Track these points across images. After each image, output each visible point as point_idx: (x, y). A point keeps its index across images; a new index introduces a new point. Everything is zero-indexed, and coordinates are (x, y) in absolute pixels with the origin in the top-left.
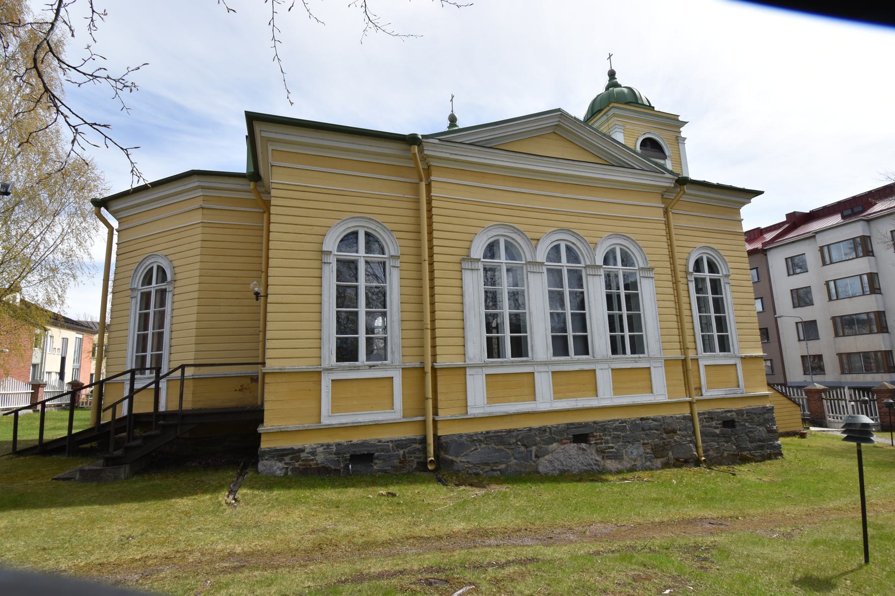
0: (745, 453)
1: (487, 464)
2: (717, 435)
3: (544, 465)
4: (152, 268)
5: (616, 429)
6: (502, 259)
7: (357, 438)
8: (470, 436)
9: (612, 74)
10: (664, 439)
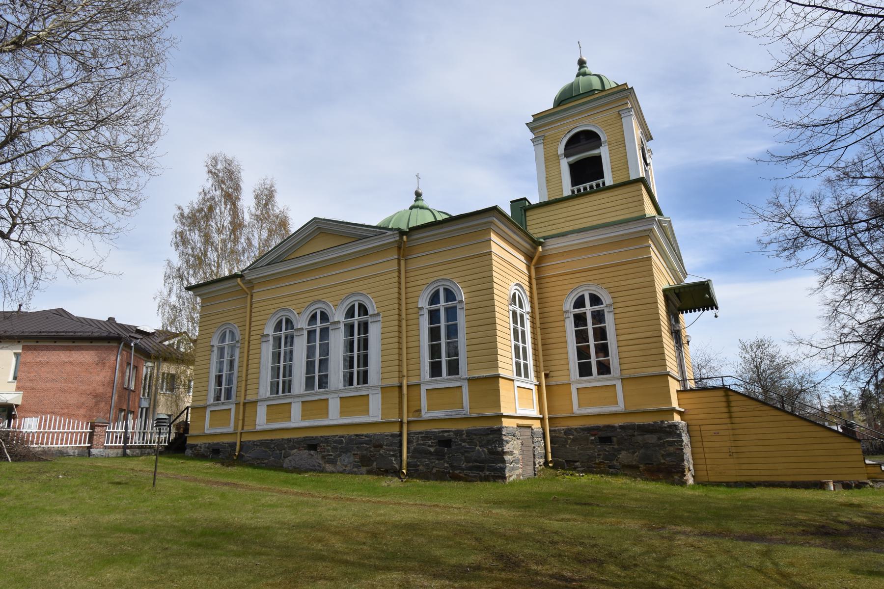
0: (457, 472)
2: (430, 453)
3: (286, 463)
5: (335, 442)
6: (442, 304)
7: (216, 440)
8: (254, 442)
9: (582, 63)
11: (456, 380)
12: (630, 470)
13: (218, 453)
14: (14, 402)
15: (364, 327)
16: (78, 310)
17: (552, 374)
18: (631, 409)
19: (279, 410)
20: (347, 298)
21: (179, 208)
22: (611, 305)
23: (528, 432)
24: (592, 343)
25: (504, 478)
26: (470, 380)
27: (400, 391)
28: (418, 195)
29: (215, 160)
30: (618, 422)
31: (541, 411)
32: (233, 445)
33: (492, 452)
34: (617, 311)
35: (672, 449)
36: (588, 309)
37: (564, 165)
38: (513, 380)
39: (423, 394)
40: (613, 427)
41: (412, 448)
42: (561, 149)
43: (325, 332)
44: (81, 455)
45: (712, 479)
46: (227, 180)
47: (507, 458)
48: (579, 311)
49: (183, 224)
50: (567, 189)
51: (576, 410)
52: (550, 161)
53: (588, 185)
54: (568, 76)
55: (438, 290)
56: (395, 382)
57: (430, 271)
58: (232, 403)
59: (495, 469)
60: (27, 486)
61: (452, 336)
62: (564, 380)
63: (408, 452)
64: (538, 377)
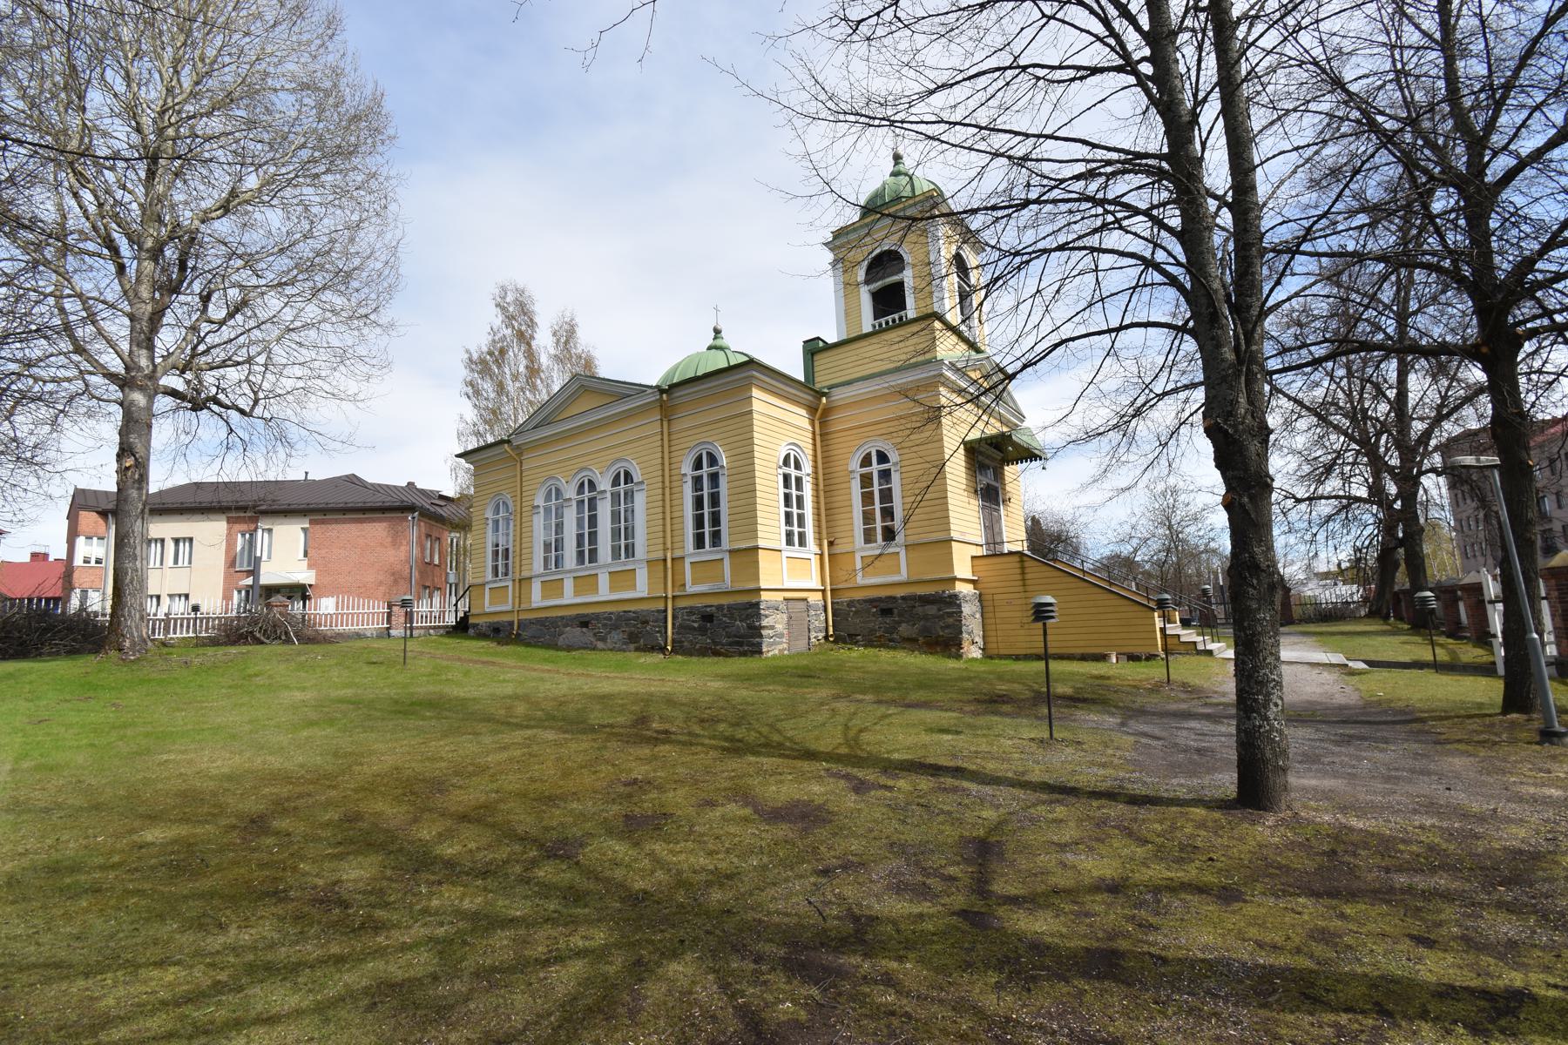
3: (561, 641)
7: (496, 619)
12: (910, 643)
13: (499, 633)
14: (307, 582)
16: (372, 475)
18: (913, 579)
19: (552, 587)
20: (613, 464)
21: (468, 351)
23: (802, 605)
25: (761, 652)
26: (730, 551)
27: (665, 565)
28: (717, 332)
29: (504, 290)
30: (899, 592)
32: (511, 624)
33: (751, 627)
35: (951, 620)
36: (875, 468)
42: (861, 274)
44: (379, 637)
45: (1002, 652)
46: (518, 315)
47: (764, 632)
48: (884, 466)
49: (472, 370)
50: (867, 323)
51: (860, 580)
52: (849, 287)
53: (889, 318)
56: (660, 555)
57: (697, 430)
59: (753, 644)
60: (282, 667)
61: (714, 508)
62: (847, 548)
64: (820, 546)
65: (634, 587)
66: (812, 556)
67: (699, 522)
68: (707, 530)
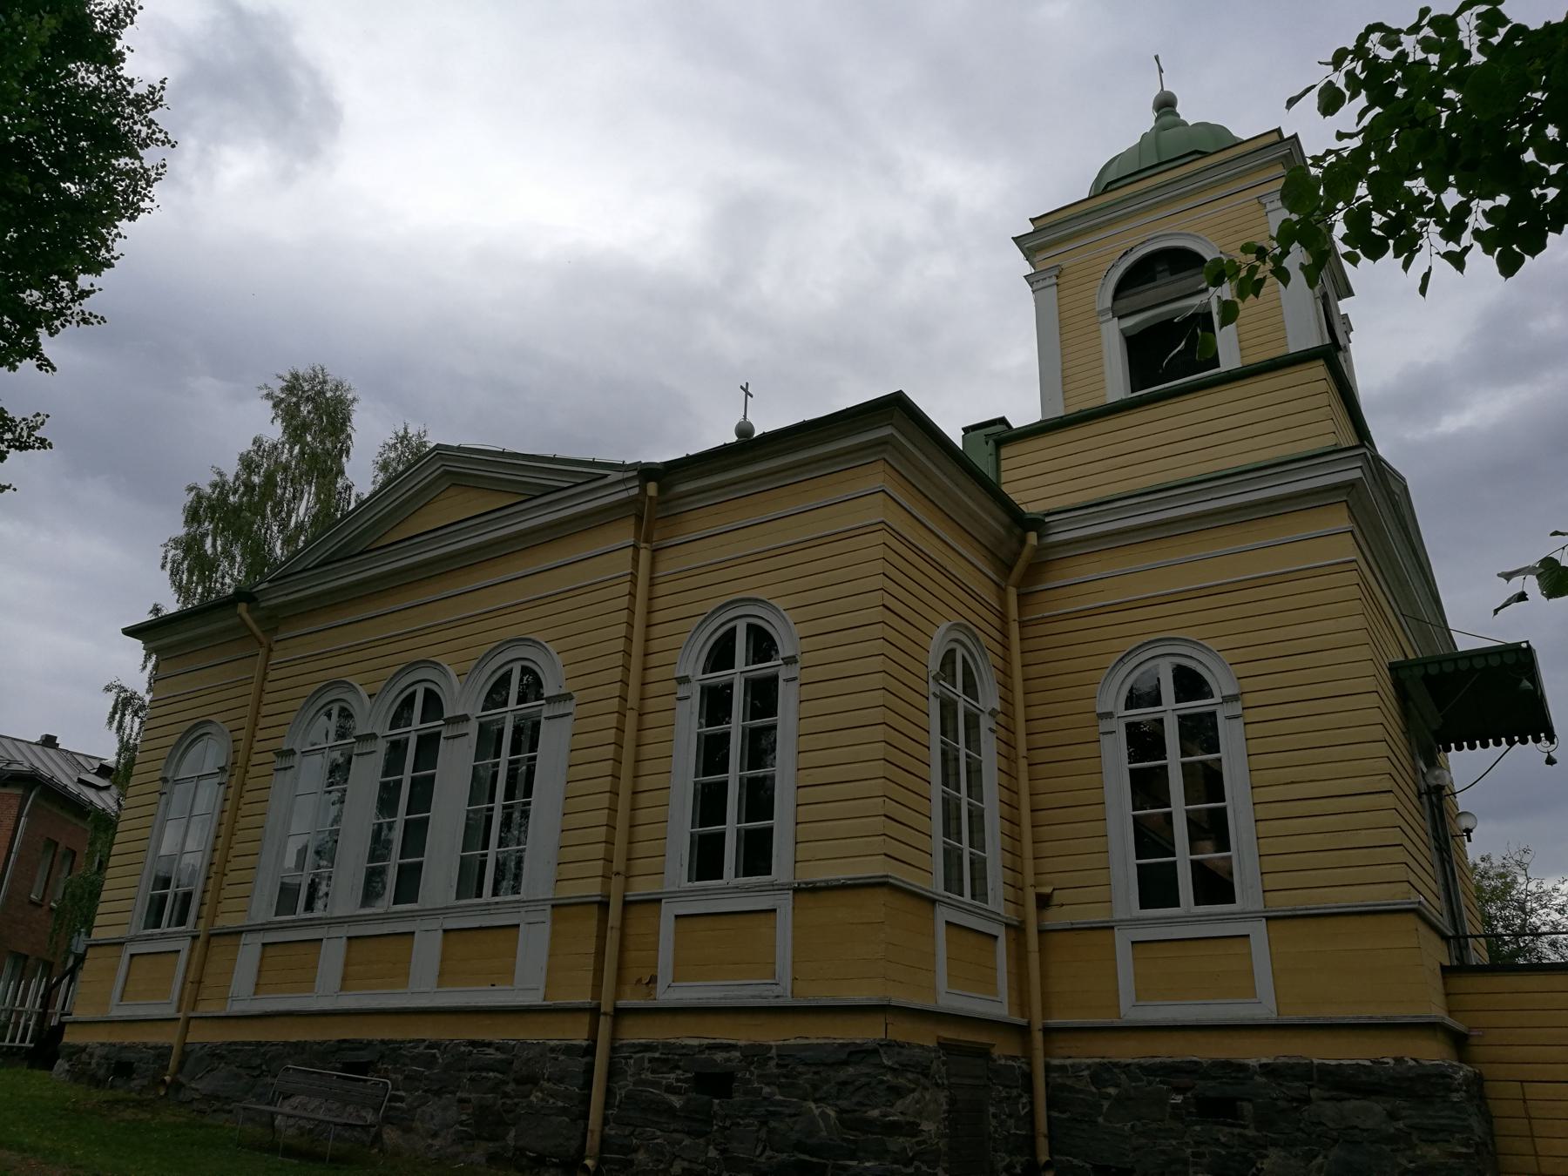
1: (217, 1098)
2: (671, 1110)
4: (731, 634)
9: (1166, 104)
10: (506, 1095)
11: (760, 889)
15: (527, 735)
17: (1058, 897)
22: (1234, 698)
24: (1179, 808)
26: (803, 890)
27: (611, 917)
30: (1256, 1053)
31: (1022, 1002)
32: (162, 1053)
34: (1252, 715)
36: (1170, 710)
37: (1111, 338)
38: (933, 902)
39: (667, 926)
40: (1242, 1067)
41: (620, 1094)
43: (429, 744)
48: (1143, 714)
50: (1115, 384)
54: (1130, 126)
55: (734, 629)
56: (593, 889)
58: (182, 935)
63: (607, 1105)
65: (508, 974)
66: (1000, 931)
67: (710, 804)
68: (732, 827)
